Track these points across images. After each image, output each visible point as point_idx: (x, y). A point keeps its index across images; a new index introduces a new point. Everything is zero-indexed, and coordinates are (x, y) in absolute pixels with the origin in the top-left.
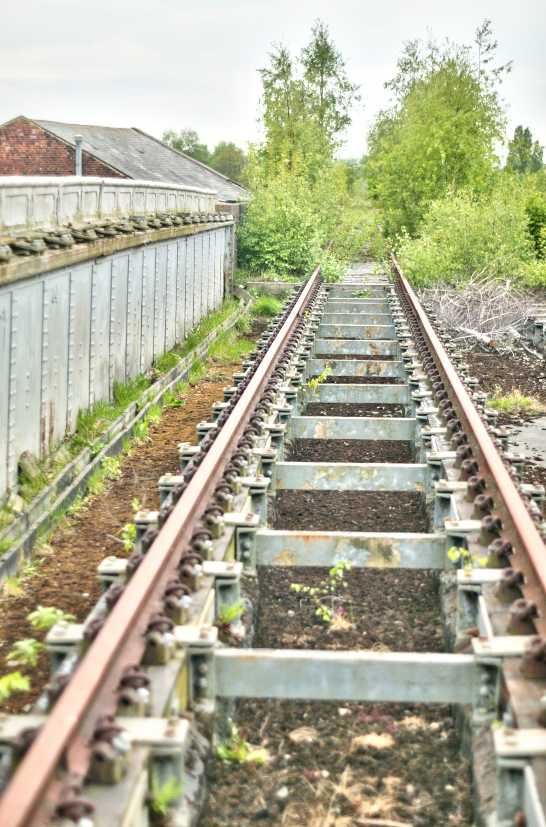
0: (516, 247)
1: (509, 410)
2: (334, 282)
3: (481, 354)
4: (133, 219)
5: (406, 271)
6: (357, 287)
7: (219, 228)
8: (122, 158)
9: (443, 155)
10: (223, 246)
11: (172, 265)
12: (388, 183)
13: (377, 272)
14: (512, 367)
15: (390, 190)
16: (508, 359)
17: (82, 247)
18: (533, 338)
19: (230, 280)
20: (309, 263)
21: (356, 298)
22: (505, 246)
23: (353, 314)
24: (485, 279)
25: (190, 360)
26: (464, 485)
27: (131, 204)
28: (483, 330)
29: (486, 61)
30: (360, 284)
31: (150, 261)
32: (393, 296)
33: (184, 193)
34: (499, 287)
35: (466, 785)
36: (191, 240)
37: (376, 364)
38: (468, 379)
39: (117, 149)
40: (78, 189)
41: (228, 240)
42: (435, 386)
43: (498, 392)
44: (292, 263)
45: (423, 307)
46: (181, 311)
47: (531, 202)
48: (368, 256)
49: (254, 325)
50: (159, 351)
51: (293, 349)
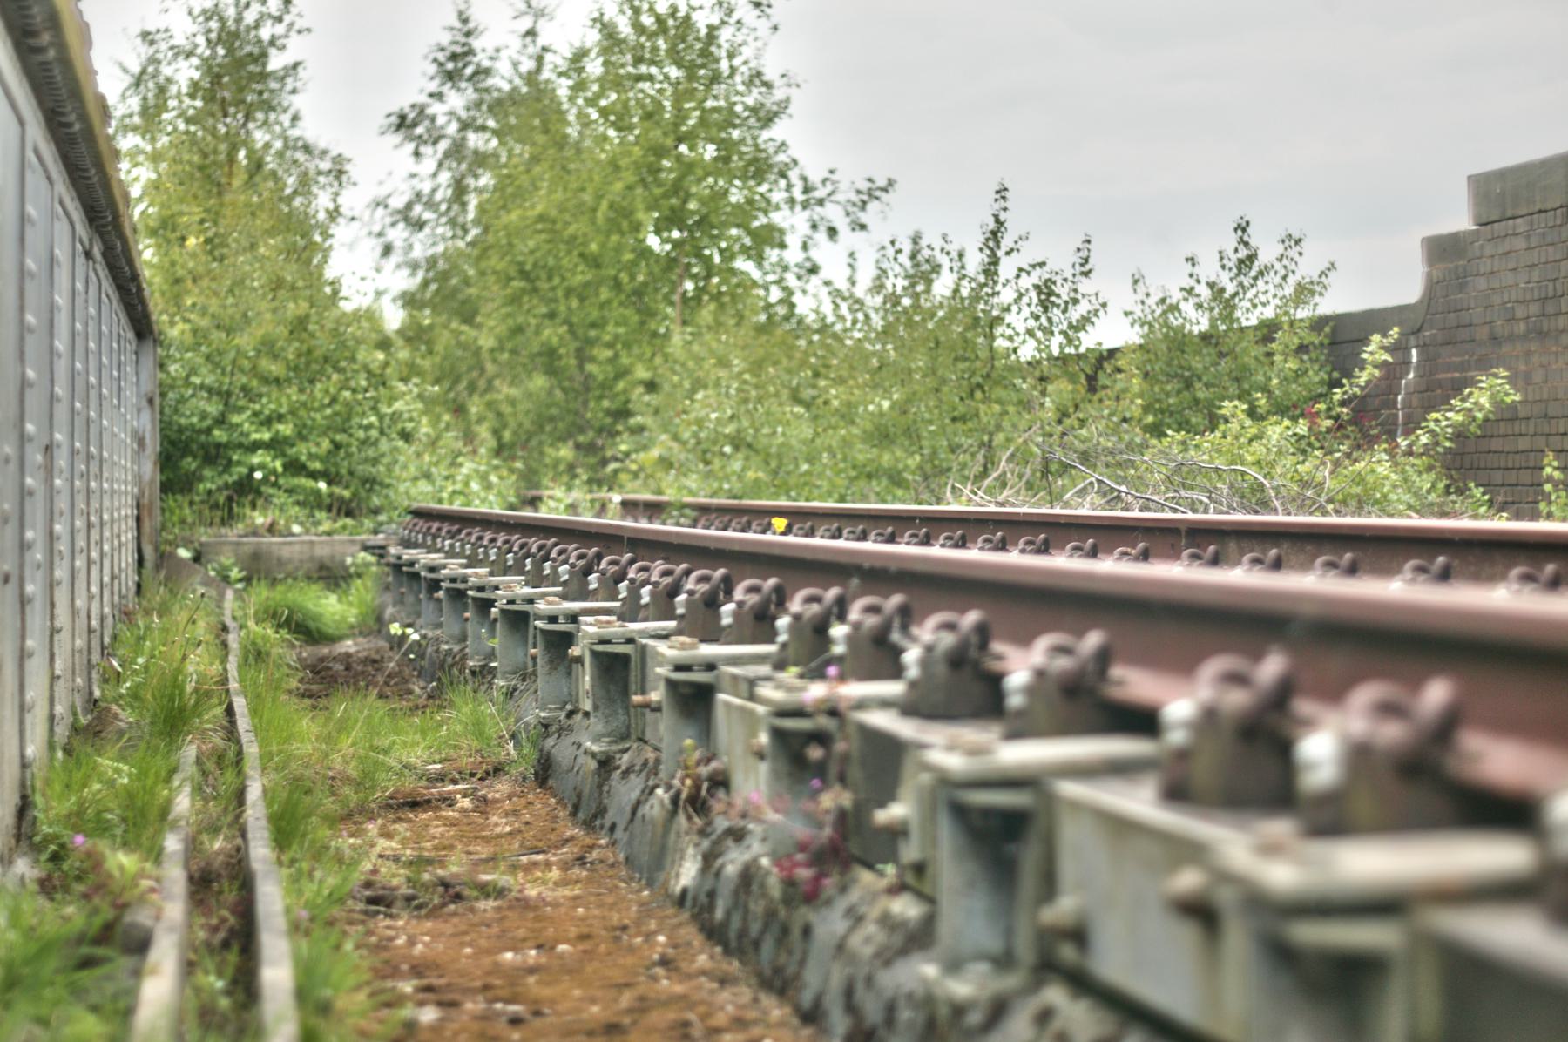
9: (190, 752)
15: (510, 322)
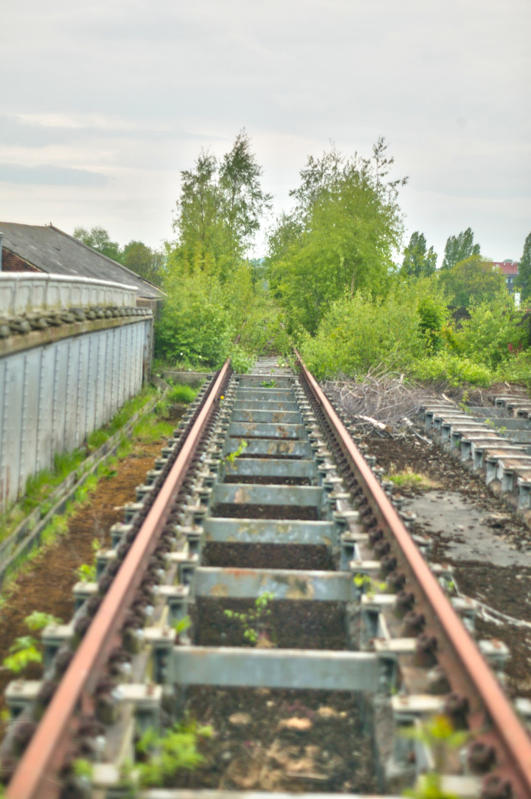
0: (409, 345)
1: (402, 485)
2: (243, 372)
3: (376, 439)
4: (73, 311)
5: (309, 364)
6: (264, 378)
7: (141, 321)
8: (40, 254)
9: (342, 259)
10: (143, 338)
11: (102, 353)
12: (293, 282)
13: (283, 365)
14: (404, 451)
16: (401, 443)
17: (36, 334)
18: (425, 426)
19: (149, 370)
20: (221, 355)
21: (263, 388)
22: (398, 343)
23: (261, 401)
24: (381, 373)
25: (117, 438)
26: (366, 536)
27: (70, 297)
28: (378, 418)
29: (382, 175)
30: (267, 375)
31: (85, 349)
32: (298, 387)
33: (112, 289)
34: (394, 380)
35: (369, 752)
36: (117, 331)
37: (285, 444)
38: (367, 456)
39: (35, 246)
40: (29, 283)
41: (148, 332)
42: (339, 461)
43: (392, 469)
44: (204, 355)
45: (327, 397)
46: (108, 395)
47: (424, 305)
48: (273, 350)
49: (172, 411)
50: (90, 429)
51: (213, 428)
